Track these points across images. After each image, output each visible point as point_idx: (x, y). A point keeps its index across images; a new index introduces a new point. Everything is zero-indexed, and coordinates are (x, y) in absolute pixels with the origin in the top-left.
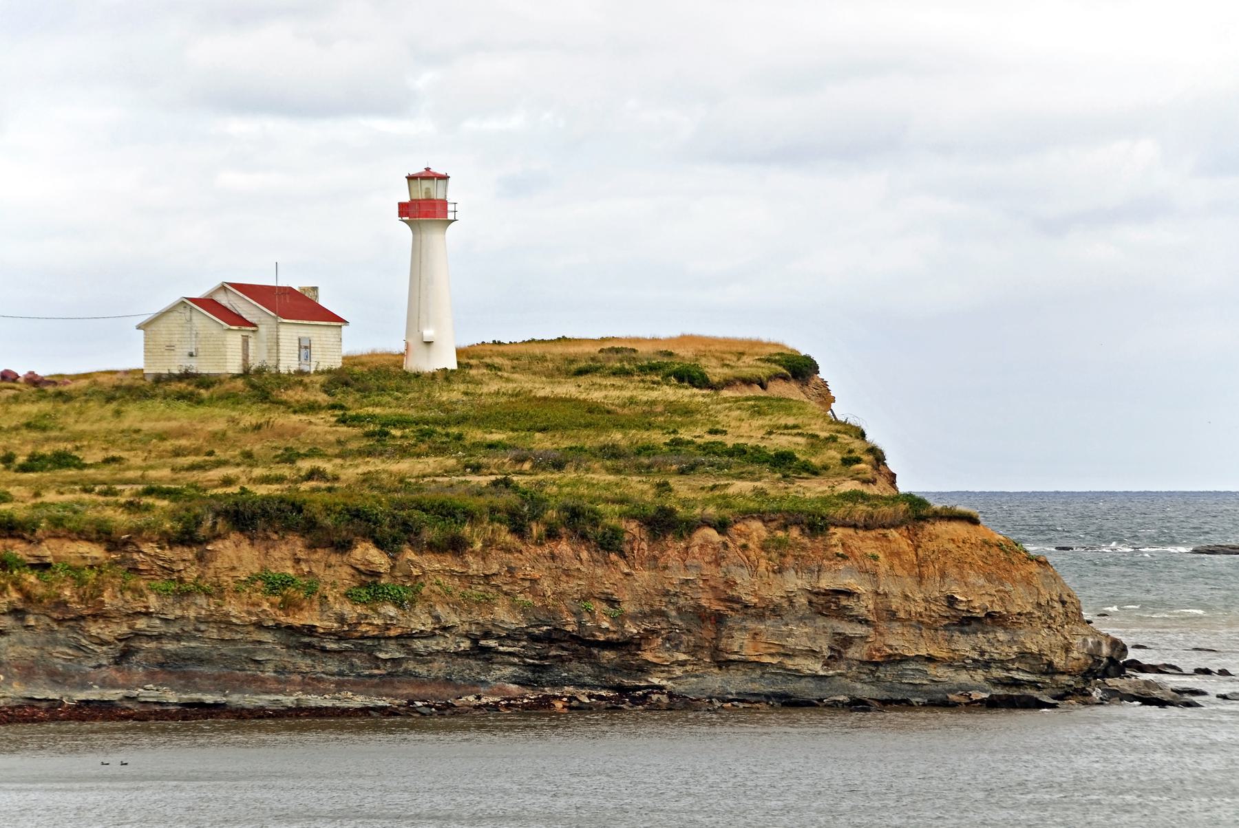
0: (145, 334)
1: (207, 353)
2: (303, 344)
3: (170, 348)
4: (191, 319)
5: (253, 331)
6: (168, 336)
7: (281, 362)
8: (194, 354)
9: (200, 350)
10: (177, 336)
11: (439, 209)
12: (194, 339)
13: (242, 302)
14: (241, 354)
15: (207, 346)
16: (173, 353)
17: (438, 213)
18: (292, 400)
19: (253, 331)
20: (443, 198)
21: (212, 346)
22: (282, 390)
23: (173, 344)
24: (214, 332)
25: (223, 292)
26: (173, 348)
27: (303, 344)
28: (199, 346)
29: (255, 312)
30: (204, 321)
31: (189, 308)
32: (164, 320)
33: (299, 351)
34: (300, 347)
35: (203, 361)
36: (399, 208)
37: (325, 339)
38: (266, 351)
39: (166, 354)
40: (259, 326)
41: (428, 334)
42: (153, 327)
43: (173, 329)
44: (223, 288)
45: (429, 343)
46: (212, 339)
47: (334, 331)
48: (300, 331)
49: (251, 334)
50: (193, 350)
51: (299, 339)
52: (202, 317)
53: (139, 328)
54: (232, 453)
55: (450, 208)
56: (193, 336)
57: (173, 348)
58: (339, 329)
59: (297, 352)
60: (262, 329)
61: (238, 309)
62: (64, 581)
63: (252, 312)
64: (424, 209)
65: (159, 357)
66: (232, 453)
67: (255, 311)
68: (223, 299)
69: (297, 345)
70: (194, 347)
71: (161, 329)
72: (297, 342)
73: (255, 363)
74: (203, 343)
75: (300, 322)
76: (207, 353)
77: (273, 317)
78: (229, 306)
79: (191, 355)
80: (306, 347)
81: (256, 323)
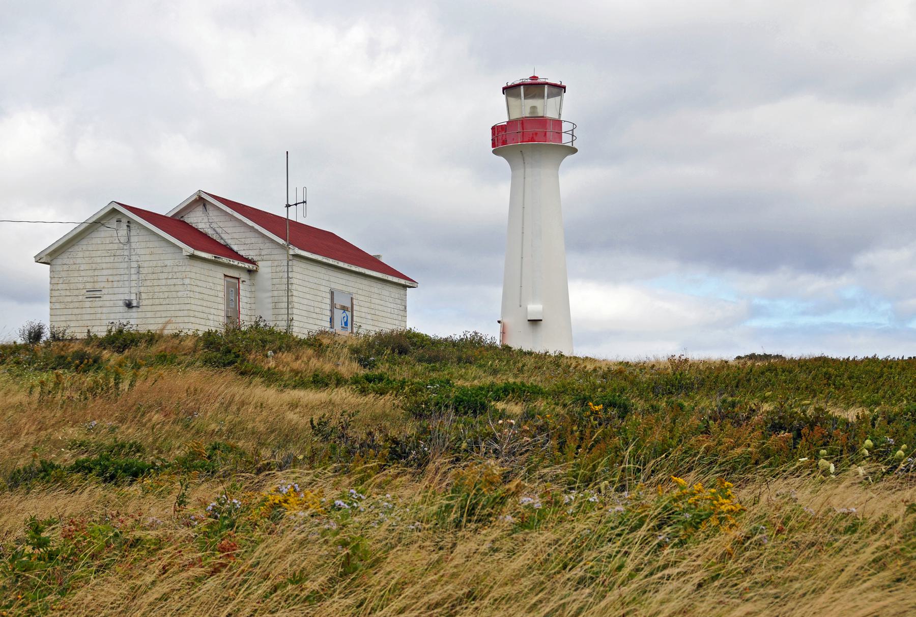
0: (51, 271)
1: (157, 302)
2: (339, 301)
3: (94, 294)
4: (129, 241)
5: (250, 271)
6: (91, 273)
7: (295, 323)
8: (134, 304)
9: (144, 296)
10: (105, 272)
11: (550, 129)
12: (134, 277)
13: (230, 224)
14: (222, 307)
15: (157, 289)
16: (98, 303)
17: (550, 135)
18: (286, 369)
19: (250, 271)
20: (556, 117)
21: (164, 289)
22: (269, 353)
23: (98, 286)
24: (169, 263)
25: (201, 208)
26: (98, 294)
27: (340, 301)
28: (142, 289)
29: (253, 240)
30: (151, 245)
31: (124, 220)
32: (84, 245)
33: (332, 311)
34: (333, 306)
35: (149, 315)
36: (493, 134)
37: (377, 301)
38: (271, 306)
39: (88, 304)
40: (260, 264)
41: (535, 309)
42: (64, 259)
43: (98, 260)
44: (200, 201)
45: (535, 322)
46: (164, 276)
47: (395, 292)
48: (332, 279)
49: (244, 276)
50: (133, 297)
51: (332, 293)
52: (155, 244)
53: (39, 259)
54: (734, 533)
55: (565, 127)
56: (133, 271)
57: (98, 294)
58: (402, 292)
59: (329, 313)
60: (264, 268)
61: (224, 236)
62: (506, 478)
63: (248, 241)
64: (530, 130)
65: (76, 311)
66: (734, 533)
67: (252, 239)
68: (198, 220)
69: (328, 301)
70: (134, 290)
71: (79, 261)
72: (329, 296)
73: (246, 320)
74: (148, 283)
75: (331, 261)
76: (157, 302)
77: (282, 246)
78: (210, 232)
79: (129, 305)
80: (344, 308)
81: (255, 258)
